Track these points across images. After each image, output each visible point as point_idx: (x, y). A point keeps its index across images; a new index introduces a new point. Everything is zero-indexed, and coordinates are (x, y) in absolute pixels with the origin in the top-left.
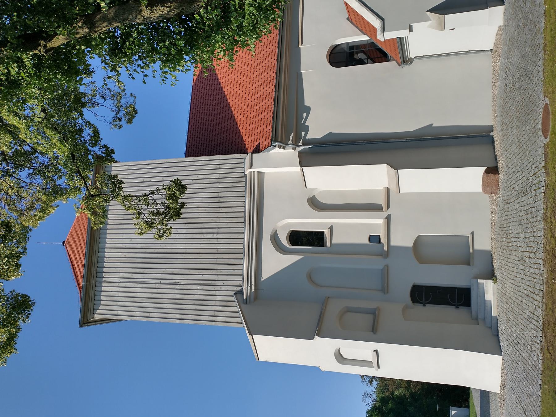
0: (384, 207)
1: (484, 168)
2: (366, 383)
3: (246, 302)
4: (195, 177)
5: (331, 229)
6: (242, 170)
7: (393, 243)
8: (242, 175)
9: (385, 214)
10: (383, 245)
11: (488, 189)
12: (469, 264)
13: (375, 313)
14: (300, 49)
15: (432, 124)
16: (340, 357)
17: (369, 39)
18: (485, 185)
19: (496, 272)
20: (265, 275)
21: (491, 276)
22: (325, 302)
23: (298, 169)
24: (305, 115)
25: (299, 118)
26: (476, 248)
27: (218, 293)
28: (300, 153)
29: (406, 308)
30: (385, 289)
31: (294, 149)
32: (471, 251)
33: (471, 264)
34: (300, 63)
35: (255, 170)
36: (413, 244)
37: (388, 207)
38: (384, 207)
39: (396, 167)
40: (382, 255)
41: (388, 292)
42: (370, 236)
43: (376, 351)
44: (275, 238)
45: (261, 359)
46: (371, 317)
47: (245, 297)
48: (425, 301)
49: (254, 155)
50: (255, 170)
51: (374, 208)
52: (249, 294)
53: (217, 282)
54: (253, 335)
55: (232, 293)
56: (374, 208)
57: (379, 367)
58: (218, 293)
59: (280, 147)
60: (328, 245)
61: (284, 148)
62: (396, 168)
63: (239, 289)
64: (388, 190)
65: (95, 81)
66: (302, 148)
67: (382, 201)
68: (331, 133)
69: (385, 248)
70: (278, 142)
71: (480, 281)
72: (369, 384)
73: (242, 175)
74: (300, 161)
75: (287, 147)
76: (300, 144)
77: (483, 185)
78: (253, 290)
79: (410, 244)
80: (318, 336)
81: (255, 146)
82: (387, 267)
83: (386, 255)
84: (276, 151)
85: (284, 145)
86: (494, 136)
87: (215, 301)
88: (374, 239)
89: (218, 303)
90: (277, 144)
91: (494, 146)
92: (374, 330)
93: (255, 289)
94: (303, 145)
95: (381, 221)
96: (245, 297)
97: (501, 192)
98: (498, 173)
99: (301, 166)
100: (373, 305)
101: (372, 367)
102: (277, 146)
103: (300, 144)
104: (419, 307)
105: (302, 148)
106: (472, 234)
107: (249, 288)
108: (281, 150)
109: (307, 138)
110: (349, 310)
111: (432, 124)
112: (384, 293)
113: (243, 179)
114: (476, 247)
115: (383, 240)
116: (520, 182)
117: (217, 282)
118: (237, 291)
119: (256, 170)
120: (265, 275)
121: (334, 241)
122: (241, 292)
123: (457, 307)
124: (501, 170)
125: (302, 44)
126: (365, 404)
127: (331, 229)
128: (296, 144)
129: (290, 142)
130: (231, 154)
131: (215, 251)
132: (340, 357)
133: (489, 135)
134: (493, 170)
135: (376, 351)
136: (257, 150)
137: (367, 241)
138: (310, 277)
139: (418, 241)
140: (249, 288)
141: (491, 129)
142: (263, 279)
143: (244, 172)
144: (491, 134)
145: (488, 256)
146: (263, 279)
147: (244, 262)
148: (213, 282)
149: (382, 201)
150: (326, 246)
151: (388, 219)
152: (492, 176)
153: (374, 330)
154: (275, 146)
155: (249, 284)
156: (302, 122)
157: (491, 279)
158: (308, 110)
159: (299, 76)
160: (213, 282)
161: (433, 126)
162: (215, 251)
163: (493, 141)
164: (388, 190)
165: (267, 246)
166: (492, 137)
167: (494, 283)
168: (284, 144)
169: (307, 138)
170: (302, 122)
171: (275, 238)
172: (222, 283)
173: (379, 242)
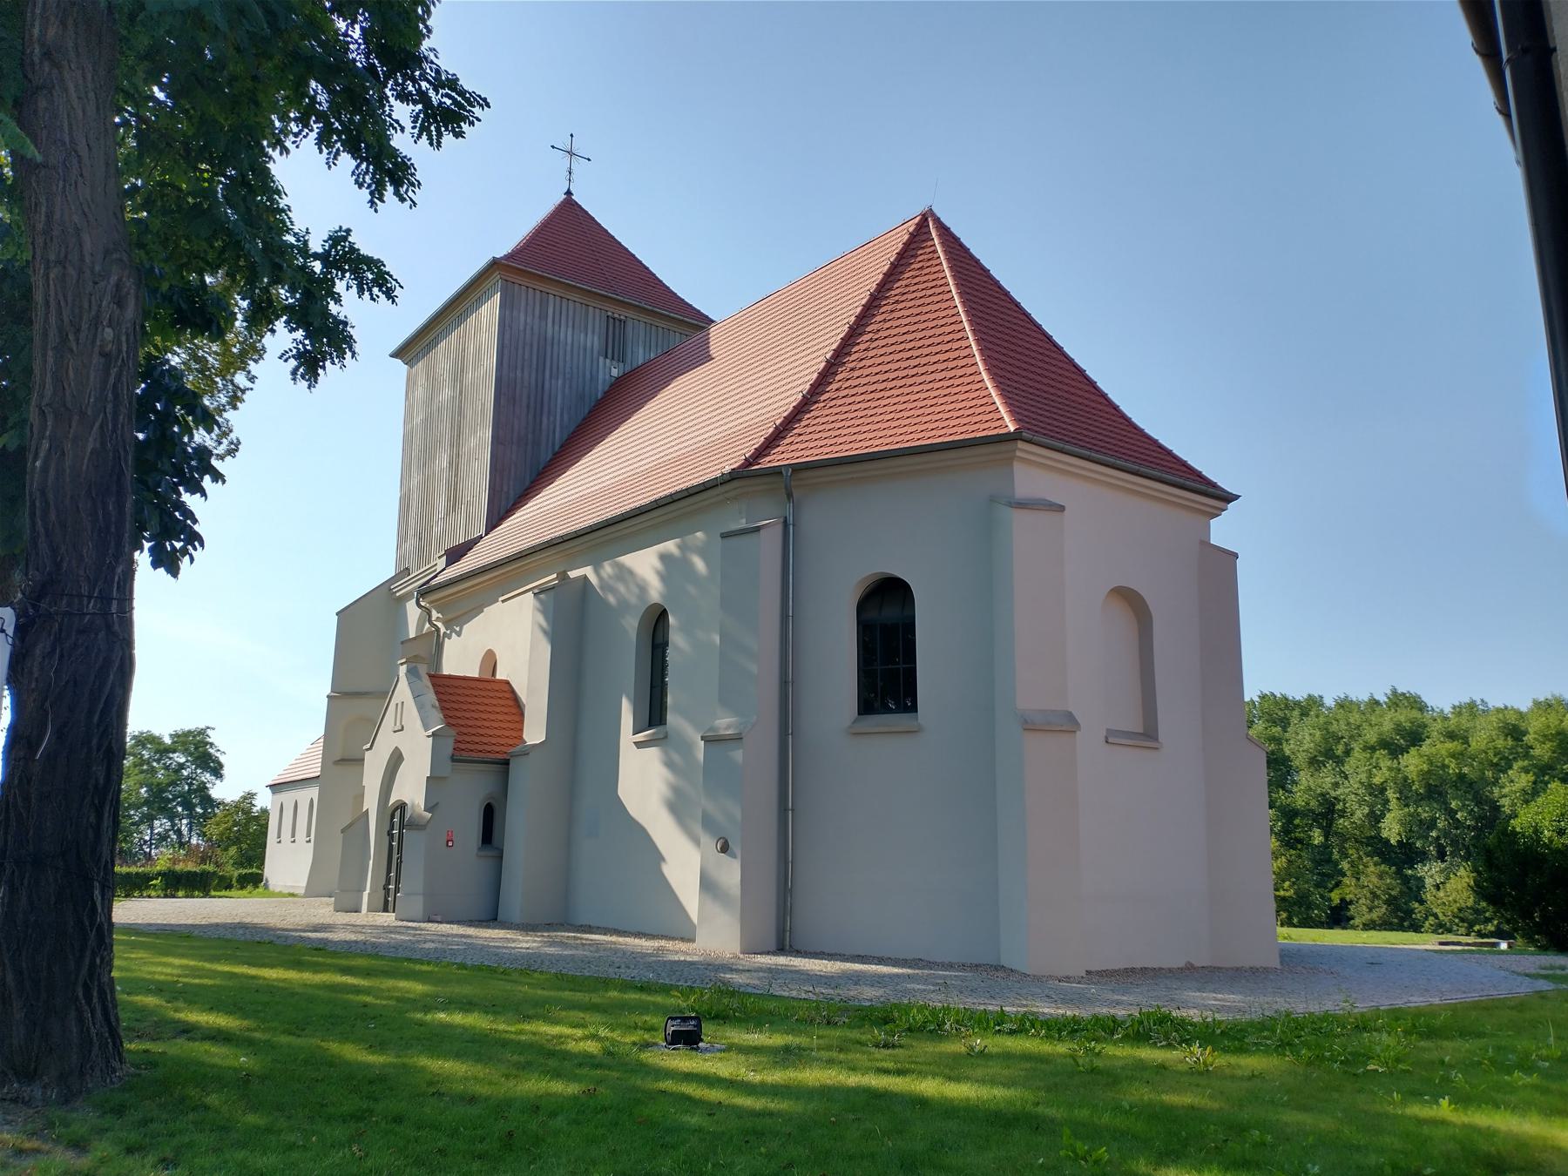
47: (392, 587)
96: (392, 587)
125: (503, 601)
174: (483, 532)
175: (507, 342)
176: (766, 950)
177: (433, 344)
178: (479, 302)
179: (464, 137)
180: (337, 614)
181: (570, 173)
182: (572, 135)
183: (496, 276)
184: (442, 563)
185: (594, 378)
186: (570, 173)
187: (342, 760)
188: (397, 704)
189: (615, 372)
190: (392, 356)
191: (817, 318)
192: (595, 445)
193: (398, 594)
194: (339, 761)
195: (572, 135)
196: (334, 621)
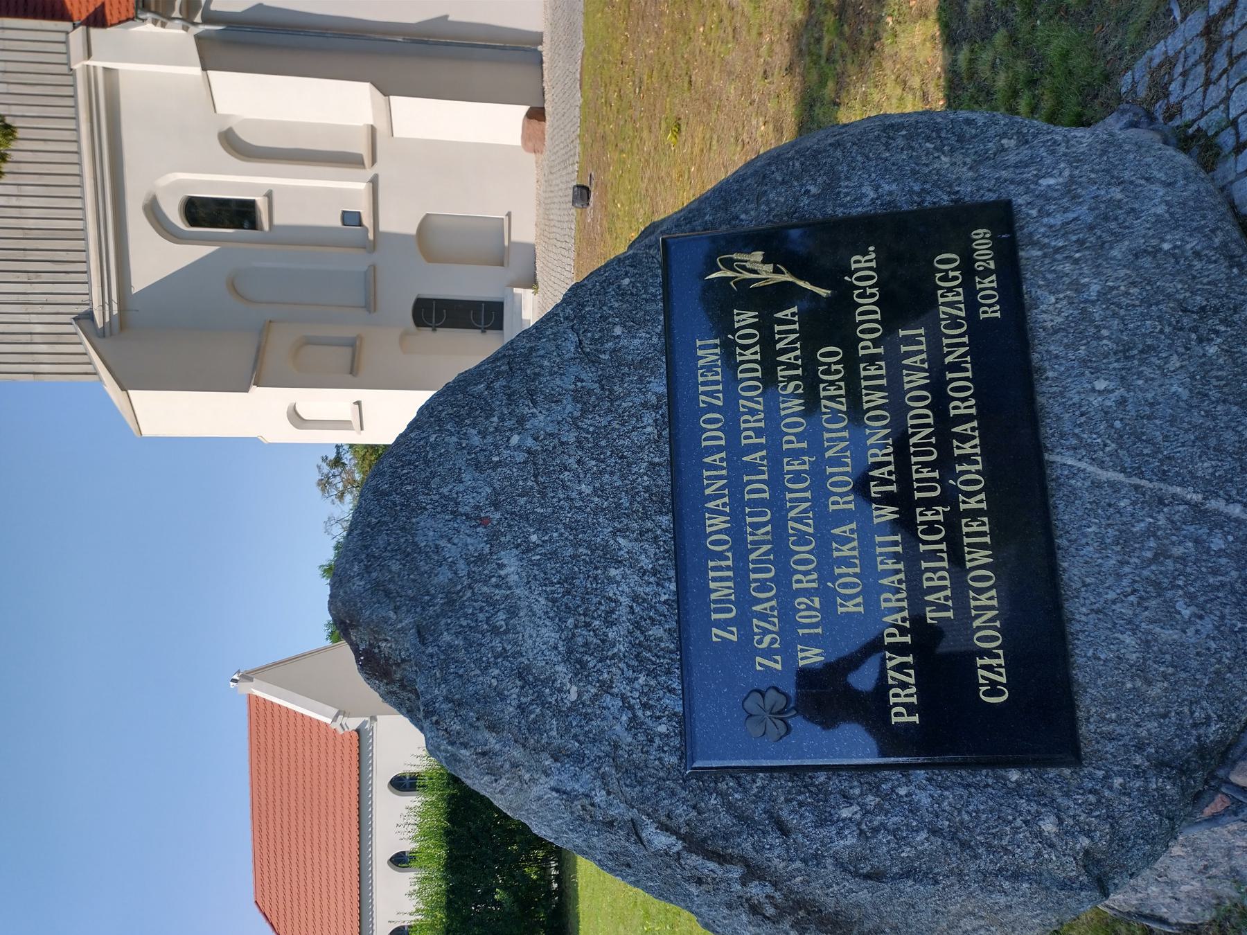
0: (367, 161)
1: (525, 109)
2: (330, 499)
3: (102, 334)
5: (269, 196)
6: (63, 59)
7: (383, 227)
8: (64, 69)
9: (369, 173)
10: (367, 230)
11: (530, 144)
12: (502, 265)
13: (354, 345)
16: (295, 418)
18: (526, 137)
19: (539, 278)
20: (139, 282)
21: (532, 283)
23: (197, 71)
27: (34, 318)
28: (198, 38)
30: (370, 304)
31: (186, 29)
32: (506, 243)
33: (505, 264)
35: (97, 63)
36: (232, 158)
37: (374, 161)
38: (367, 161)
39: (386, 89)
40: (364, 248)
42: (344, 212)
43: (358, 403)
44: (153, 211)
45: (146, 432)
46: (347, 351)
47: (100, 324)
48: (436, 322)
49: (95, 32)
50: (97, 63)
51: (346, 160)
52: (107, 320)
53: (31, 298)
54: (129, 391)
55: (68, 318)
56: (346, 160)
57: (362, 429)
58: (34, 318)
59: (155, 22)
60: (266, 227)
61: (163, 25)
62: (386, 93)
63: (84, 309)
64: (373, 130)
66: (202, 28)
67: (363, 149)
68: (260, 6)
69: (371, 236)
70: (149, 11)
71: (517, 291)
72: (337, 501)
73: (64, 69)
74: (201, 58)
75: (169, 23)
76: (198, 19)
77: (523, 137)
78: (115, 312)
79: (413, 230)
80: (258, 384)
81: (92, 9)
82: (374, 268)
83: (371, 247)
84: (147, 29)
85: (164, 20)
86: (544, 53)
87: (31, 333)
88: (352, 219)
89: (37, 338)
90: (149, 16)
91: (542, 68)
92: (353, 370)
93: (119, 310)
94: (206, 21)
95: (362, 186)
97: (546, 153)
98: (544, 120)
99: (204, 69)
100: (348, 332)
101: (352, 429)
102: (150, 19)
103: (198, 19)
104: (426, 332)
105: (202, 28)
106: (509, 215)
107: (107, 307)
108: (158, 29)
110: (309, 342)
111: (447, 16)
112: (370, 312)
113: (68, 80)
114: (514, 238)
115: (367, 221)
116: (562, 145)
117: (31, 298)
118: (79, 314)
119: (100, 64)
120: (139, 282)
121: (277, 221)
122: (89, 316)
123: (483, 332)
124: (548, 118)
126: (331, 537)
127: (269, 196)
128: (188, 20)
129: (176, 14)
130: (35, 17)
131: (19, 234)
132: (295, 418)
133: (536, 50)
134: (537, 114)
135: (358, 403)
136: (98, 19)
137: (338, 223)
138: (233, 287)
139: (425, 225)
140: (107, 307)
141: (538, 38)
142: (134, 291)
143: (68, 64)
144: (540, 48)
145: (530, 250)
146: (134, 291)
147: (88, 256)
148: (22, 298)
149: (363, 149)
150: (262, 229)
151: (374, 182)
152: (534, 122)
153: (353, 370)
154: (144, 20)
155: (107, 300)
157: (530, 287)
160: (22, 298)
161: (450, 19)
162: (19, 234)
163: (542, 62)
164: (373, 130)
165: (138, 227)
166: (540, 54)
167: (535, 293)
168: (163, 15)
171: (153, 211)
172: (43, 298)
173: (360, 224)
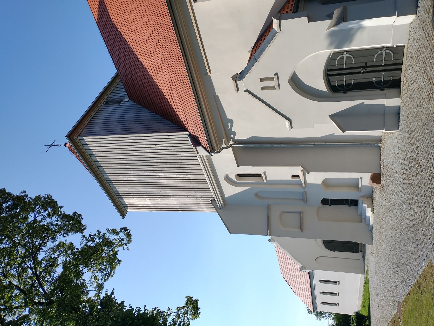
3: (220, 208)
4: (154, 146)
14: (210, 76)
15: (334, 134)
17: (273, 19)
22: (269, 207)
24: (229, 124)
25: (225, 127)
26: (363, 184)
29: (319, 208)
34: (214, 88)
41: (307, 202)
47: (219, 207)
65: (130, 305)
93: (223, 202)
96: (219, 207)
109: (236, 138)
111: (334, 134)
125: (210, 72)
156: (229, 129)
158: (232, 122)
159: (216, 98)
161: (335, 135)
169: (236, 138)
170: (229, 129)
174: (185, 135)
175: (104, 133)
176: (379, 150)
177: (114, 188)
178: (87, 149)
179: (112, 293)
180: (231, 234)
181: (58, 145)
182: (44, 146)
183: (76, 139)
184: (199, 148)
185: (128, 106)
186: (58, 145)
187: (301, 228)
188: (263, 88)
189: (127, 100)
190: (123, 218)
191: (118, 40)
192: (148, 73)
193: (222, 203)
194: (301, 230)
195: (44, 146)
196: (233, 235)
